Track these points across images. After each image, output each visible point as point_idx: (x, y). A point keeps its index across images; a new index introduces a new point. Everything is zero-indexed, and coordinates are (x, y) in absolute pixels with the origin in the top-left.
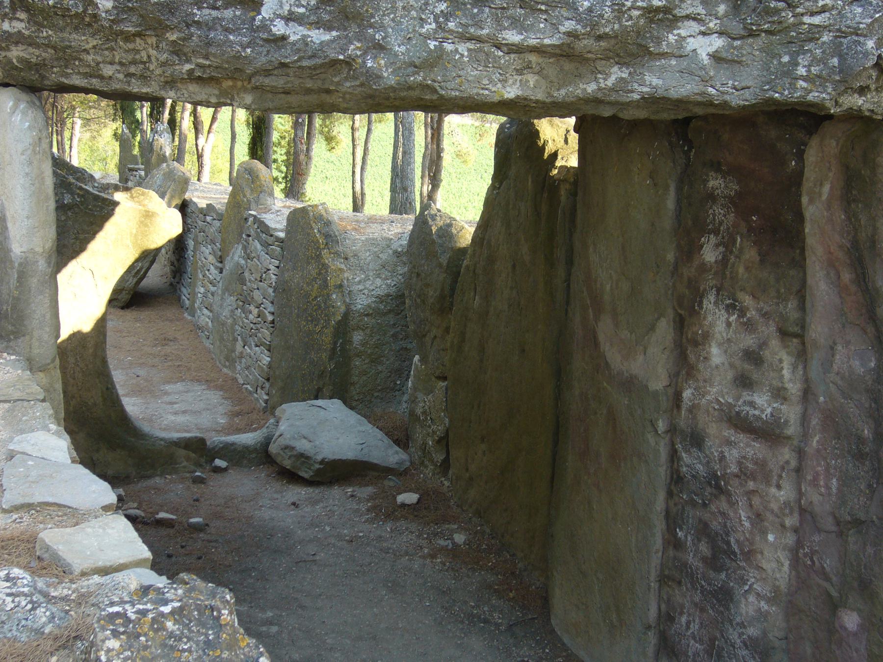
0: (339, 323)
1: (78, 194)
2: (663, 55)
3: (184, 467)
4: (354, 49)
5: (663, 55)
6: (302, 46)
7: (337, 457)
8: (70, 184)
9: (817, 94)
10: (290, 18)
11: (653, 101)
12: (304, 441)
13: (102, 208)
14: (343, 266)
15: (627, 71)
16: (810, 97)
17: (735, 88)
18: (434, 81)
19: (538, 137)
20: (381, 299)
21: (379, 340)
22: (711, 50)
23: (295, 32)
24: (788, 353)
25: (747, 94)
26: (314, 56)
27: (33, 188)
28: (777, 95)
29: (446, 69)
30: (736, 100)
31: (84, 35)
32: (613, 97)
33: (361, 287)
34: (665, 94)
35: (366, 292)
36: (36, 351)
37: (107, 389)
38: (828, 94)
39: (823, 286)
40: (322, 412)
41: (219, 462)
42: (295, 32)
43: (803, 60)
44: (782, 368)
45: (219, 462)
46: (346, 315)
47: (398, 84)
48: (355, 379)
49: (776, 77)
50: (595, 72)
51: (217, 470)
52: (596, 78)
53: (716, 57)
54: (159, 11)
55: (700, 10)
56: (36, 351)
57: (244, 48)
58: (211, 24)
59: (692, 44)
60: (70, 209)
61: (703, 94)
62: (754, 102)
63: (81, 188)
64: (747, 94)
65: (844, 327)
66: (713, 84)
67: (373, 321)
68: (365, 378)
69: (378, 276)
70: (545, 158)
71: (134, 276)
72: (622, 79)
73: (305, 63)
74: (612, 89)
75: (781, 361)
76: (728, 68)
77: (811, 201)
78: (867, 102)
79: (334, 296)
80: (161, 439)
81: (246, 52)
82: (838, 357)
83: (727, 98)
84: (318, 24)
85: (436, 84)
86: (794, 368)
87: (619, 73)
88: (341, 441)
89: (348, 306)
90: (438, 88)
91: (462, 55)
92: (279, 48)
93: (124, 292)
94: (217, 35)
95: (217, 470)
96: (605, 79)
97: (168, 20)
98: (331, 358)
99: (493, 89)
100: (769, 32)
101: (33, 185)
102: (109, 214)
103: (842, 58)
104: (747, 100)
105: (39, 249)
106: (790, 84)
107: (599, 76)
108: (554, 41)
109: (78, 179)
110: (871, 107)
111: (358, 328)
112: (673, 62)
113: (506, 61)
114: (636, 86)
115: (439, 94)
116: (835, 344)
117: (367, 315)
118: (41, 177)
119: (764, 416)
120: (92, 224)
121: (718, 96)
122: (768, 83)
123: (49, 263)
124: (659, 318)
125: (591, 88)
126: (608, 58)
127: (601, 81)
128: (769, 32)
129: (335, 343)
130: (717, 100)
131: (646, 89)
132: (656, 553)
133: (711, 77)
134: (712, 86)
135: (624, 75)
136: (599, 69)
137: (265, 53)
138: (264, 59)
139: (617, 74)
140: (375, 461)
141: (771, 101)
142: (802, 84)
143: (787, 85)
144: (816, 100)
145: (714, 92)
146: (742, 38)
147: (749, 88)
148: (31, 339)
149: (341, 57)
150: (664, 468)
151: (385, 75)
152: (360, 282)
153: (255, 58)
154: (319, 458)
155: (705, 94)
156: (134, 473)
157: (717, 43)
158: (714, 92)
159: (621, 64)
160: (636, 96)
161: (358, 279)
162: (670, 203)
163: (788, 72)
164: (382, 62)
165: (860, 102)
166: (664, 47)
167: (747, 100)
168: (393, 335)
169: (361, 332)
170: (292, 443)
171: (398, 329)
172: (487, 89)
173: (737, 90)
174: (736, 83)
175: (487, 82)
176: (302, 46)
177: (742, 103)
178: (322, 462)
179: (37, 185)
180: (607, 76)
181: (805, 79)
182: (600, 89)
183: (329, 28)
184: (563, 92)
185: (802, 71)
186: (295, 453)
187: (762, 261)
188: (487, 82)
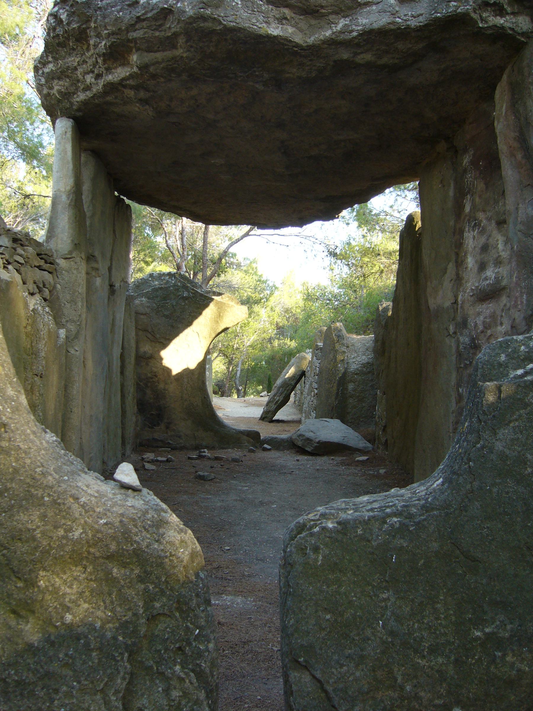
1: (192, 293)
3: (246, 446)
6: (147, 5)
7: (327, 440)
8: (188, 287)
9: (462, 8)
12: (311, 433)
13: (204, 301)
14: (345, 350)
15: (349, 20)
16: (459, 11)
17: (413, 16)
18: (219, 16)
19: (414, 221)
20: (364, 365)
21: (363, 388)
24: (502, 235)
25: (421, 19)
26: (152, 10)
27: (60, 156)
28: (439, 15)
29: (226, 10)
30: (413, 23)
31: (73, 57)
32: (342, 37)
33: (354, 360)
34: (371, 27)
35: (357, 362)
36: (60, 246)
37: (205, 398)
38: (471, 5)
39: (510, 172)
41: (266, 446)
44: (498, 244)
45: (266, 446)
46: (345, 374)
47: (195, 14)
48: (349, 410)
49: (438, 4)
50: (330, 23)
52: (331, 27)
54: (83, 8)
56: (60, 246)
57: (118, 12)
58: (106, 7)
60: (186, 299)
61: (393, 23)
62: (426, 22)
63: (193, 290)
64: (421, 19)
65: (522, 191)
66: (399, 15)
67: (360, 377)
68: (355, 410)
69: (364, 355)
70: (417, 230)
71: (275, 404)
72: (346, 24)
73: (149, 15)
74: (341, 32)
75: (497, 240)
76: (408, 6)
77: (498, 122)
78: (507, 21)
79: (339, 365)
80: (234, 429)
81: (119, 14)
82: (520, 212)
83: (409, 23)
85: (221, 18)
86: (506, 243)
87: (344, 22)
88: (333, 435)
89: (346, 369)
90: (222, 20)
91: (237, 4)
92: (135, 8)
93: (270, 413)
95: (265, 450)
96: (336, 27)
97: (88, 12)
98: (336, 398)
99: (260, 26)
101: (60, 154)
104: (421, 22)
106: (446, 6)
107: (333, 25)
109: (193, 286)
110: (511, 26)
111: (351, 381)
112: (374, 7)
113: (266, 8)
114: (354, 27)
115: (223, 24)
116: (518, 205)
117: (356, 374)
118: (65, 151)
119: (491, 282)
120: (198, 308)
121: (403, 23)
122: (433, 10)
123: (68, 198)
124: (448, 264)
125: (328, 33)
126: (336, 13)
127: (334, 28)
129: (338, 390)
130: (403, 25)
131: (359, 28)
132: (452, 413)
133: (397, 12)
134: (399, 18)
135: (347, 23)
136: (332, 20)
137: (129, 13)
138: (128, 17)
139: (342, 23)
140: (351, 445)
141: (437, 19)
143: (445, 7)
144: (463, 11)
145: (400, 20)
147: (422, 15)
148: (58, 238)
149: (166, 6)
150: (455, 356)
151: (187, 10)
152: (354, 358)
153: (124, 17)
154: (317, 440)
155: (394, 22)
156: (217, 446)
158: (400, 20)
159: (344, 17)
160: (355, 34)
161: (353, 356)
162: (451, 193)
164: (186, 4)
165: (502, 22)
167: (421, 22)
168: (371, 386)
169: (353, 384)
170: (304, 433)
171: (374, 383)
172: (255, 25)
173: (415, 17)
174: (413, 13)
175: (255, 21)
176: (147, 5)
177: (418, 24)
178: (319, 442)
179: (63, 155)
182: (333, 33)
184: (312, 39)
186: (304, 438)
187: (487, 188)
188: (255, 21)
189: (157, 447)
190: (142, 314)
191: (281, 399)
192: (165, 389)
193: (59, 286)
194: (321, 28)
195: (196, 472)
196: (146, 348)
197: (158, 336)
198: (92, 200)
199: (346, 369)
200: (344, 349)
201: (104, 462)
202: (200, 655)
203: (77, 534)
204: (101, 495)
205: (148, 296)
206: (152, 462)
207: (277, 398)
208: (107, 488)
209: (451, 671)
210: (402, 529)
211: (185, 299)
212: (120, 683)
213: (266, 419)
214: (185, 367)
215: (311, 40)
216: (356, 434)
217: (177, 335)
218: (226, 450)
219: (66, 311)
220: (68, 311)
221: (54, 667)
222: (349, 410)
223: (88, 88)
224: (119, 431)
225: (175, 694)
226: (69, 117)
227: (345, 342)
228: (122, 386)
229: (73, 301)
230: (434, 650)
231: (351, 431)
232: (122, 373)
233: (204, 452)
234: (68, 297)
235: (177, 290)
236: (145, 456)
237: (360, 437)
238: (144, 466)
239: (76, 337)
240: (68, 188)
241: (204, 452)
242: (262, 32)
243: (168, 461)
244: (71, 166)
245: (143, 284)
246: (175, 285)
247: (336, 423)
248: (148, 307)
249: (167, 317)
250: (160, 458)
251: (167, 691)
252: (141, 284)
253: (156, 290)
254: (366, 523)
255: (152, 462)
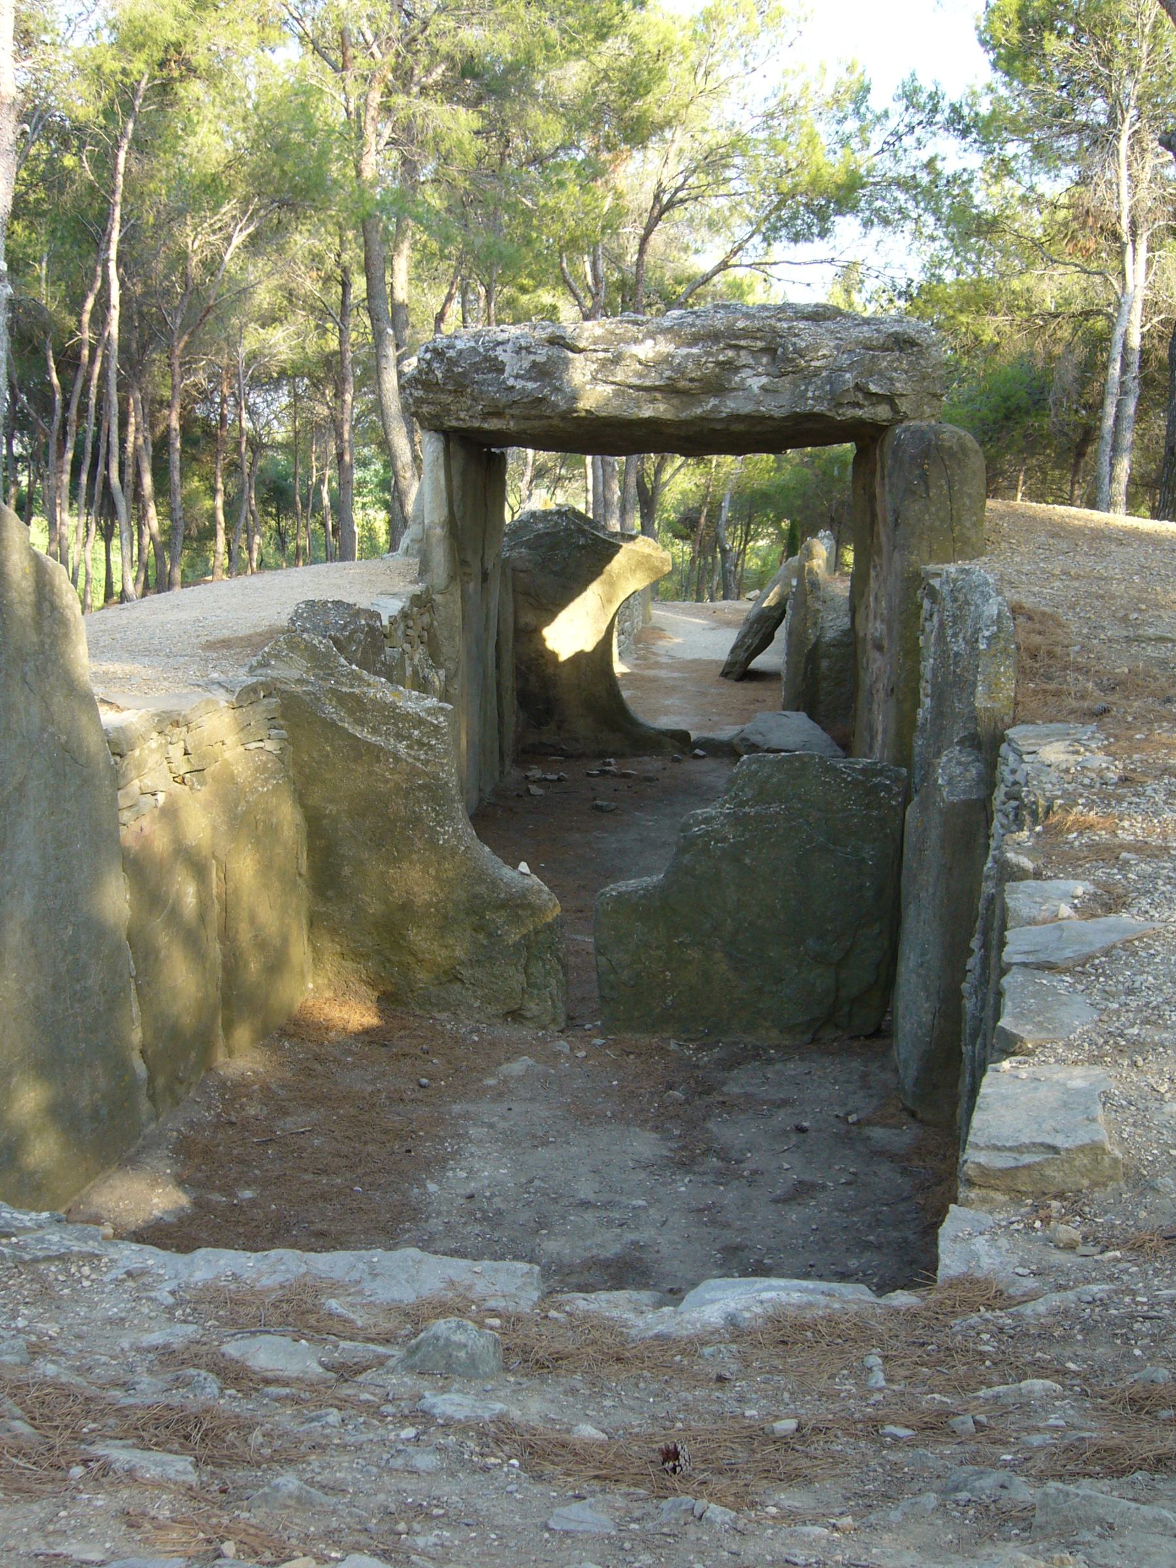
0: (810, 651)
2: (734, 389)
4: (546, 391)
5: (734, 389)
10: (517, 377)
11: (735, 418)
14: (820, 608)
22: (760, 384)
23: (519, 384)
30: (777, 413)
32: (712, 416)
36: (436, 581)
40: (785, 719)
41: (698, 751)
42: (519, 384)
43: (811, 388)
45: (698, 751)
46: (816, 645)
48: (822, 698)
50: (700, 402)
51: (696, 757)
53: (763, 388)
55: (751, 361)
56: (436, 581)
59: (749, 381)
73: (525, 400)
74: (711, 411)
84: (530, 379)
94: (484, 388)
95: (696, 757)
100: (793, 373)
102: (617, 552)
103: (832, 384)
105: (437, 521)
108: (661, 383)
118: (437, 480)
125: (699, 411)
126: (706, 393)
128: (793, 373)
129: (806, 668)
139: (713, 402)
141: (796, 413)
142: (810, 402)
146: (779, 377)
157: (764, 380)
159: (716, 396)
160: (724, 415)
163: (803, 395)
166: (733, 385)
180: (708, 403)
181: (812, 399)
183: (536, 381)
185: (810, 394)
189: (546, 754)
190: (522, 571)
191: (757, 641)
192: (554, 675)
193: (435, 623)
194: (692, 404)
195: (595, 799)
196: (528, 618)
197: (544, 601)
198: (463, 496)
199: (819, 638)
200: (818, 606)
201: (480, 790)
202: (558, 950)
203: (502, 896)
204: (513, 878)
205: (529, 545)
206: (539, 782)
207: (749, 641)
208: (514, 874)
209: (665, 956)
210: (644, 896)
211: (583, 547)
212: (523, 961)
213: (730, 676)
214: (578, 650)
215: (683, 415)
216: (825, 736)
217: (571, 599)
218: (640, 759)
219: (444, 650)
220: (446, 649)
221: (493, 954)
222: (822, 698)
223: (458, 419)
224: (497, 744)
225: (548, 967)
226: (436, 431)
227: (821, 594)
228: (498, 684)
229: (451, 638)
230: (657, 948)
231: (818, 731)
232: (498, 666)
233: (609, 764)
234: (446, 634)
235: (570, 536)
236: (529, 774)
237: (830, 741)
238: (528, 790)
239: (455, 675)
240: (442, 519)
241: (609, 764)
242: (634, 417)
243: (560, 780)
244: (444, 495)
245: (521, 528)
246: (566, 529)
247: (799, 720)
248: (530, 561)
249: (555, 574)
250: (549, 777)
251: (544, 966)
252: (522, 526)
253: (539, 537)
254: (629, 893)
255: (539, 782)
